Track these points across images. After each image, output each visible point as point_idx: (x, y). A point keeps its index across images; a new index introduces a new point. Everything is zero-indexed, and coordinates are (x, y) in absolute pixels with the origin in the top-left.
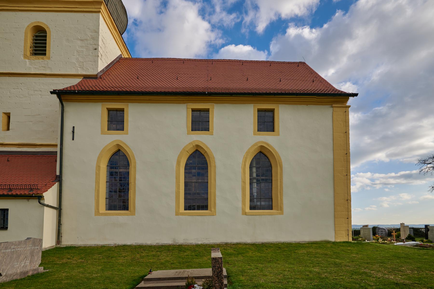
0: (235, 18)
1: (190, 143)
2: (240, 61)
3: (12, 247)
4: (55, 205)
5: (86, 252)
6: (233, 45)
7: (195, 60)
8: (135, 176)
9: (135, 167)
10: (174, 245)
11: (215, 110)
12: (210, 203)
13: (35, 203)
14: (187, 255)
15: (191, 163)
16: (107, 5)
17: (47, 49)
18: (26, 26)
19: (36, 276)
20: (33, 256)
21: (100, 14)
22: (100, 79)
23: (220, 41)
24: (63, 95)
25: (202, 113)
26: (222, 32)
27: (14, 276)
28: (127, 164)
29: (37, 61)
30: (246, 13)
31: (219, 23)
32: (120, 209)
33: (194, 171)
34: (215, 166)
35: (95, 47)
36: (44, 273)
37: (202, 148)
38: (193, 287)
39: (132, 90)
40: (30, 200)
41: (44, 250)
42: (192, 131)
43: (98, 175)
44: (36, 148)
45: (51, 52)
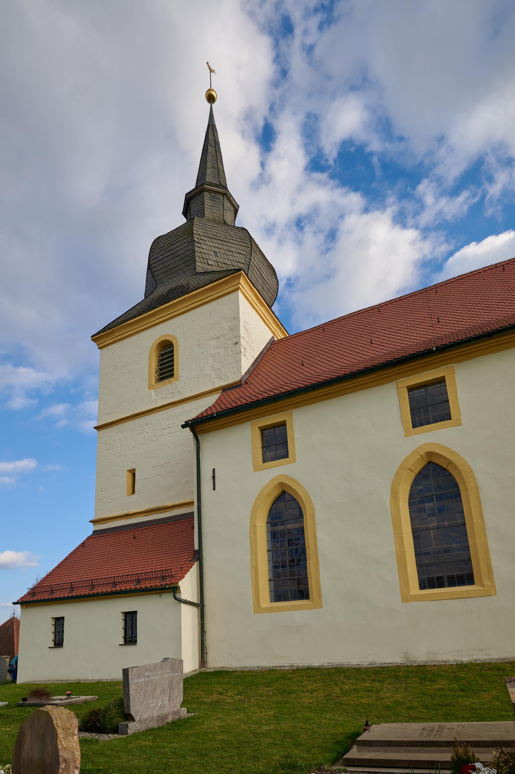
0: (468, 198)
1: (412, 453)
2: (496, 266)
3: (146, 674)
4: (195, 600)
5: (246, 683)
6: (473, 244)
7: (400, 299)
8: (315, 533)
9: (313, 518)
10: (408, 667)
11: (456, 375)
12: (478, 568)
13: (168, 598)
14: (440, 690)
15: (421, 491)
16: (247, 275)
17: (175, 367)
18: (150, 347)
19: (177, 725)
20: (173, 688)
21: (239, 292)
22: (245, 386)
23: (444, 248)
24: (198, 426)
25: (277, 430)
26: (444, 233)
27: (149, 722)
28: (298, 513)
29: (164, 387)
30: (491, 180)
31: (435, 220)
32: (294, 598)
33: (429, 505)
34: (477, 488)
35: (235, 340)
36: (188, 718)
37: (441, 456)
38: (474, 769)
39: (296, 387)
40: (163, 595)
41: (184, 677)
42: (413, 428)
43: (253, 541)
44: (167, 513)
45: (180, 370)
